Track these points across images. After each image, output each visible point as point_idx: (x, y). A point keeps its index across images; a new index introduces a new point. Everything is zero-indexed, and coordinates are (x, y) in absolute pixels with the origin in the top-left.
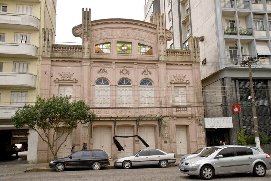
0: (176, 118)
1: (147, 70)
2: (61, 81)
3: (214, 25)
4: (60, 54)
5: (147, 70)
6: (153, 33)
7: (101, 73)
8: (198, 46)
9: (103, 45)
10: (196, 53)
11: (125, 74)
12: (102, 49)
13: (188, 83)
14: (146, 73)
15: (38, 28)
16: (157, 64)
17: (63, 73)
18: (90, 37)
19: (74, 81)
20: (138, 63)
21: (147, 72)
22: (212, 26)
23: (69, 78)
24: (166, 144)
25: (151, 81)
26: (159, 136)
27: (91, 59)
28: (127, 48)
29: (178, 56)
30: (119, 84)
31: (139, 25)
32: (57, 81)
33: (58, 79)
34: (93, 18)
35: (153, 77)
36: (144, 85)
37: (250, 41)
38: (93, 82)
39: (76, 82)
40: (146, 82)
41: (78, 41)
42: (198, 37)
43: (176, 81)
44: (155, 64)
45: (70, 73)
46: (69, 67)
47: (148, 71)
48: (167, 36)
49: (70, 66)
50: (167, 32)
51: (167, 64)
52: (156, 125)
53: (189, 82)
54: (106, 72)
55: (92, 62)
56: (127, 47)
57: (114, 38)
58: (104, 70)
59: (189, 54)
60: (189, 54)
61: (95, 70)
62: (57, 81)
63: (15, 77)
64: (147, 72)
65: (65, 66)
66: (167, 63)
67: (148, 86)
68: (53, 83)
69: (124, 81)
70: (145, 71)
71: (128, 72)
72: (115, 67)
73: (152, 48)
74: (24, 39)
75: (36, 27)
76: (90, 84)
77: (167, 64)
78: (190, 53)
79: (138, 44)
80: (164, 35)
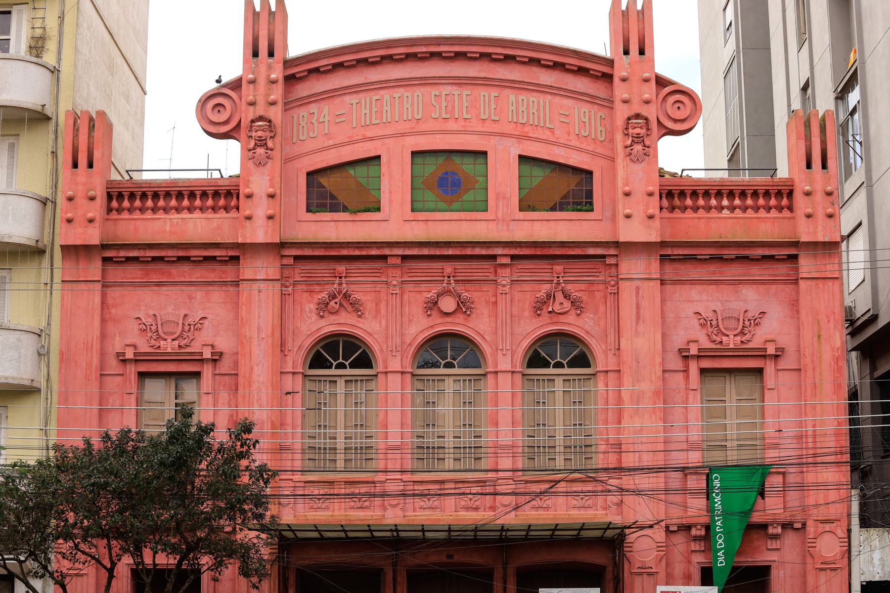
0: (779, 530)
6: (592, 99)
11: (447, 314)
14: (557, 308)
15: (49, 112)
16: (612, 261)
18: (278, 139)
19: (771, 350)
20: (404, 258)
21: (560, 304)
25: (364, 347)
32: (130, 355)
34: (300, 42)
38: (297, 359)
39: (215, 360)
41: (225, 159)
43: (712, 346)
47: (567, 296)
48: (677, 108)
51: (106, 260)
53: (782, 350)
54: (356, 307)
55: (291, 261)
58: (346, 296)
60: (785, 202)
64: (560, 304)
67: (349, 371)
68: (113, 366)
69: (447, 349)
75: (39, 109)
80: (651, 112)
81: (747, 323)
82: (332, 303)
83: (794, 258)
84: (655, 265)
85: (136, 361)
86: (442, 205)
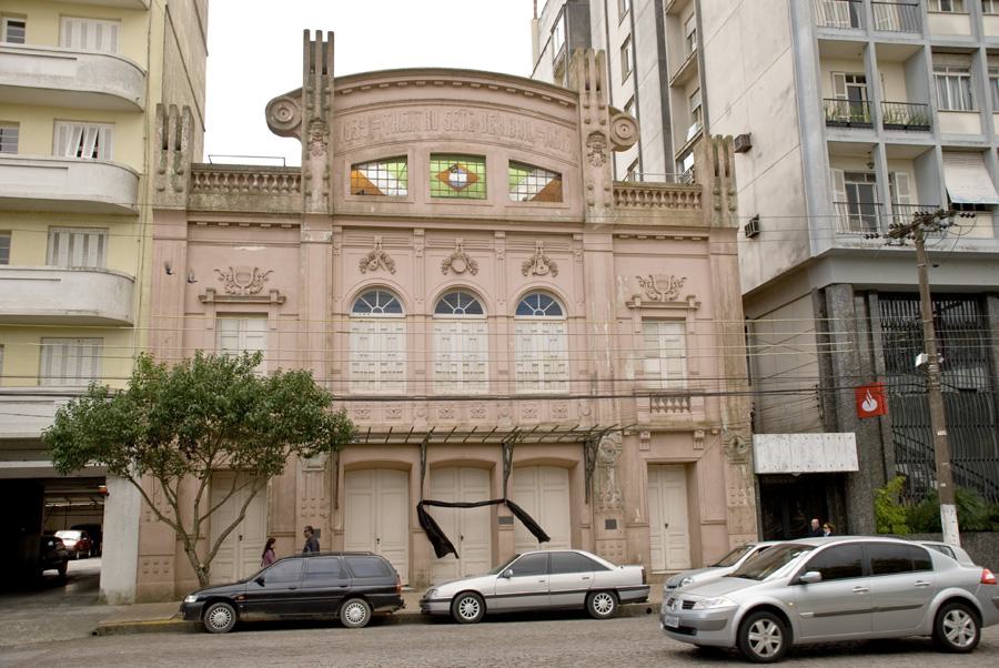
1: (543, 258)
2: (225, 297)
3: (788, 91)
4: (220, 200)
5: (543, 258)
6: (563, 122)
7: (374, 270)
8: (731, 170)
9: (380, 167)
10: (724, 195)
11: (459, 273)
12: (374, 182)
13: (692, 305)
14: (539, 271)
15: (142, 104)
16: (578, 237)
17: (231, 268)
18: (331, 137)
19: (274, 298)
20: (507, 233)
21: (541, 267)
22: (781, 97)
23: (254, 289)
24: (614, 531)
25: (555, 299)
26: (587, 502)
27: (334, 217)
28: (468, 178)
29: (656, 207)
30: (438, 311)
31: (512, 93)
32: (210, 298)
33: (215, 292)
34: (343, 66)
35: (563, 284)
36: (531, 313)
37: (920, 151)
38: (344, 303)
39: (280, 304)
40: (539, 302)
41: (288, 152)
42: (729, 138)
43: (649, 300)
44: (571, 235)
45: (256, 269)
46: (255, 248)
47: (546, 263)
48: (617, 132)
49: (259, 245)
50: (616, 117)
51: (616, 236)
52: (577, 463)
53: (698, 304)
54: (390, 266)
55: (340, 230)
56: (468, 173)
57: (421, 141)
58: (383, 257)
59: (696, 201)
60: (696, 201)
61: (352, 258)
62: (210, 298)
63: (56, 283)
64: (541, 267)
65: (240, 244)
66: (617, 232)
67: (545, 317)
68: (195, 306)
69: (459, 301)
70: (533, 262)
71: (472, 268)
72: (426, 249)
73: (559, 176)
74: (90, 144)
75: (134, 100)
76: (332, 309)
77: (616, 236)
78: (699, 195)
79: (510, 161)
80: (606, 129)
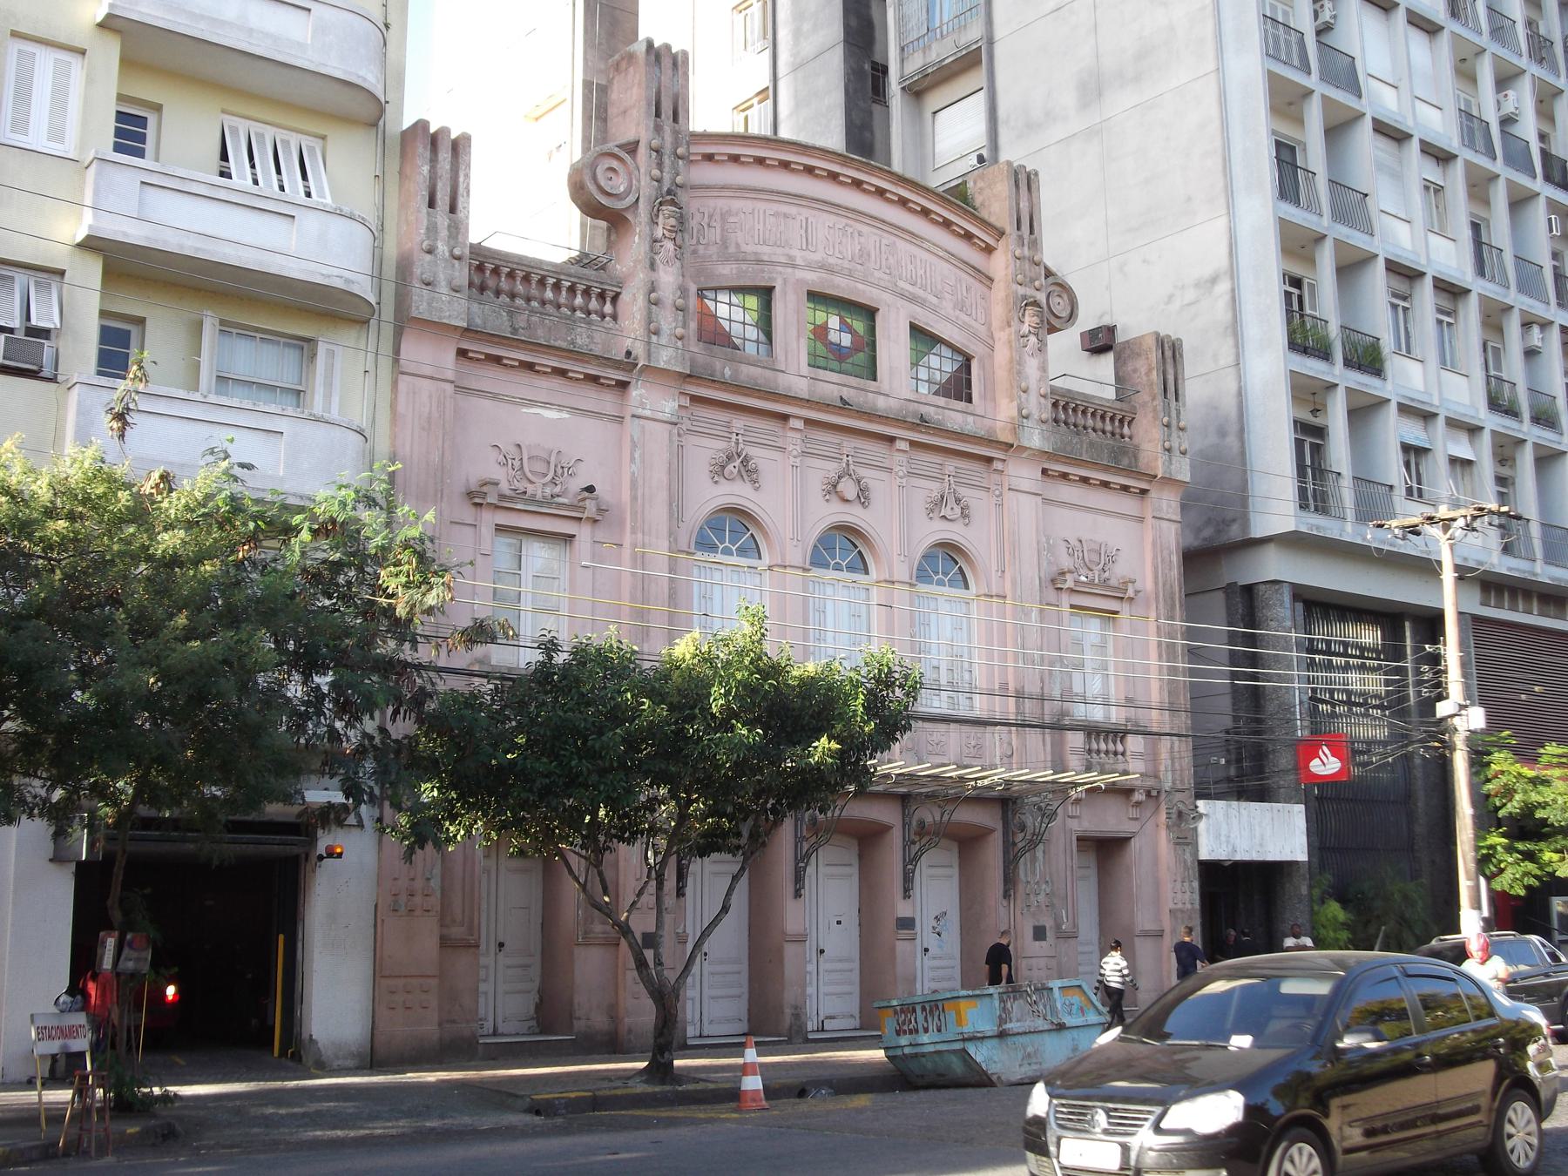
3: (1214, 280)
4: (516, 319)
8: (461, 200)
9: (734, 300)
10: (1174, 428)
12: (726, 325)
13: (1130, 593)
20: (809, 422)
22: (1197, 285)
24: (1043, 943)
26: (1006, 895)
29: (550, 308)
31: (959, 235)
35: (975, 537)
37: (1373, 401)
39: (596, 521)
40: (947, 561)
42: (444, 131)
44: (989, 460)
46: (551, 414)
47: (958, 501)
49: (560, 407)
51: (462, 353)
52: (886, 828)
57: (794, 266)
59: (608, 308)
60: (608, 308)
61: (704, 451)
63: (272, 437)
65: (532, 403)
67: (734, 560)
69: (844, 546)
73: (968, 359)
74: (237, 149)
78: (615, 299)
81: (559, 471)
82: (730, 467)
83: (623, 385)
84: (450, 356)
85: (497, 507)
86: (835, 365)
